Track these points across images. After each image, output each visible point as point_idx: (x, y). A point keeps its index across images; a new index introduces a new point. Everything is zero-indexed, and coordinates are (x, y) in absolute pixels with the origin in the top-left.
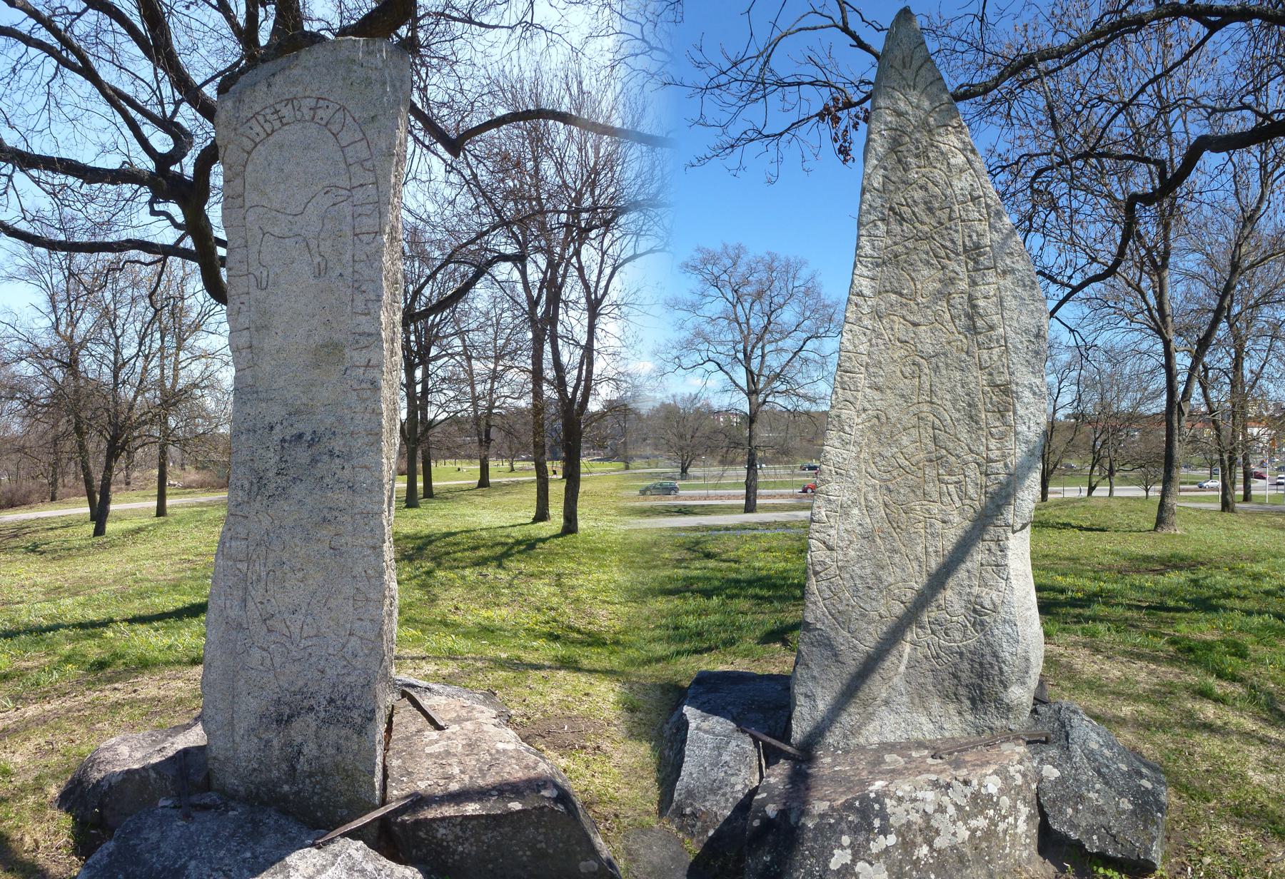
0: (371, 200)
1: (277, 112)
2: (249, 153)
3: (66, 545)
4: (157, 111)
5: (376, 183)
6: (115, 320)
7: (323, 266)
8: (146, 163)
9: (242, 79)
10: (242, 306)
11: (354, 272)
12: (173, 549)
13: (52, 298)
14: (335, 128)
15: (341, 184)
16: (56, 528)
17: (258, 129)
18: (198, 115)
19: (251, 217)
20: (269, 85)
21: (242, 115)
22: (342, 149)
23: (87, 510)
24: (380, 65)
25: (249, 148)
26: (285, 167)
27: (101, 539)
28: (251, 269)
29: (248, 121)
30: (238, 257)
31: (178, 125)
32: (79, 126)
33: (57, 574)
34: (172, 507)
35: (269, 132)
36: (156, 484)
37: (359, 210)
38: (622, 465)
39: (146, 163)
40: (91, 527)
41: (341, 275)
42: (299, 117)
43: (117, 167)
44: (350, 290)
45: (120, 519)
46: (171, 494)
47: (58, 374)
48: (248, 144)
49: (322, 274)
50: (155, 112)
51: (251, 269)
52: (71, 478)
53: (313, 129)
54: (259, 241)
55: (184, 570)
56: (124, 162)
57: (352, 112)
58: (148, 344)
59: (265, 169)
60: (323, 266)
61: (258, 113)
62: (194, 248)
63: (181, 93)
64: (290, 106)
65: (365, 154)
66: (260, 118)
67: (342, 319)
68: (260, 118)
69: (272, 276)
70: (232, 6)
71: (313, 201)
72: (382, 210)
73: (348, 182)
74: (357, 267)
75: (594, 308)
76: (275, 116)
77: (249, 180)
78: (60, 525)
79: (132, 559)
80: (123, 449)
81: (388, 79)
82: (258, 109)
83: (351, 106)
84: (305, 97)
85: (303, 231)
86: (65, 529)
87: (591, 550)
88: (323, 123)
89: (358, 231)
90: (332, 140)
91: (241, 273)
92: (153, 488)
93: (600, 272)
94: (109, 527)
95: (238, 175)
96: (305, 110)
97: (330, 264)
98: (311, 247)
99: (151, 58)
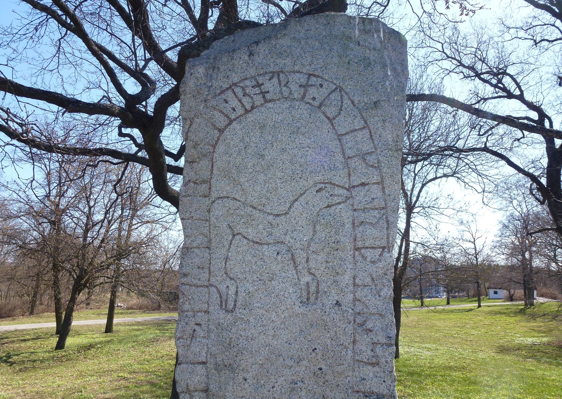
0: (376, 204)
1: (259, 85)
2: (221, 131)
3: (33, 357)
4: (131, 65)
5: (381, 183)
6: (90, 196)
7: (313, 289)
8: (118, 101)
9: (217, 44)
10: (197, 328)
11: (355, 300)
12: (114, 366)
13: (48, 174)
14: (331, 111)
15: (336, 180)
16: (28, 340)
17: (234, 103)
18: (162, 69)
19: (218, 210)
20: (251, 54)
21: (216, 84)
22: (340, 137)
23: (54, 325)
24: (379, 46)
25: (221, 125)
26: (266, 152)
27: (61, 353)
28: (213, 280)
29: (222, 92)
30: (197, 261)
31: (146, 76)
32: (78, 69)
33: (19, 387)
34: (118, 324)
35: (248, 107)
36: (108, 305)
37: (362, 216)
38: (418, 302)
39: (118, 101)
40: (55, 340)
41: (338, 303)
42: (286, 94)
43: (96, 101)
44: (350, 327)
45: (78, 334)
46: (118, 313)
47: (47, 227)
48: (221, 121)
49: (312, 299)
50: (130, 65)
51: (213, 280)
52: (47, 298)
53: (303, 110)
54: (226, 244)
55: (119, 389)
56: (104, 96)
57: (351, 95)
58: (111, 214)
59: (239, 153)
60: (313, 289)
61: (235, 85)
62: (147, 157)
63: (150, 55)
64: (275, 80)
65: (367, 147)
66: (238, 90)
67: (340, 369)
68: (238, 90)
69: (242, 295)
70: (191, 4)
71: (301, 199)
72: (391, 219)
73: (346, 180)
74: (359, 294)
75: (410, 209)
76: (257, 90)
77: (218, 164)
78: (32, 337)
79: (81, 375)
80: (85, 286)
81: (388, 62)
82: (236, 80)
83: (348, 86)
84: (294, 72)
85: (288, 238)
86: (35, 341)
87: (411, 374)
88: (316, 104)
89: (360, 244)
90: (327, 126)
91: (199, 283)
92: (105, 308)
93: (414, 186)
94: (69, 341)
95: (205, 156)
96: (294, 87)
97: (323, 286)
98: (298, 260)
99: (131, 28)
